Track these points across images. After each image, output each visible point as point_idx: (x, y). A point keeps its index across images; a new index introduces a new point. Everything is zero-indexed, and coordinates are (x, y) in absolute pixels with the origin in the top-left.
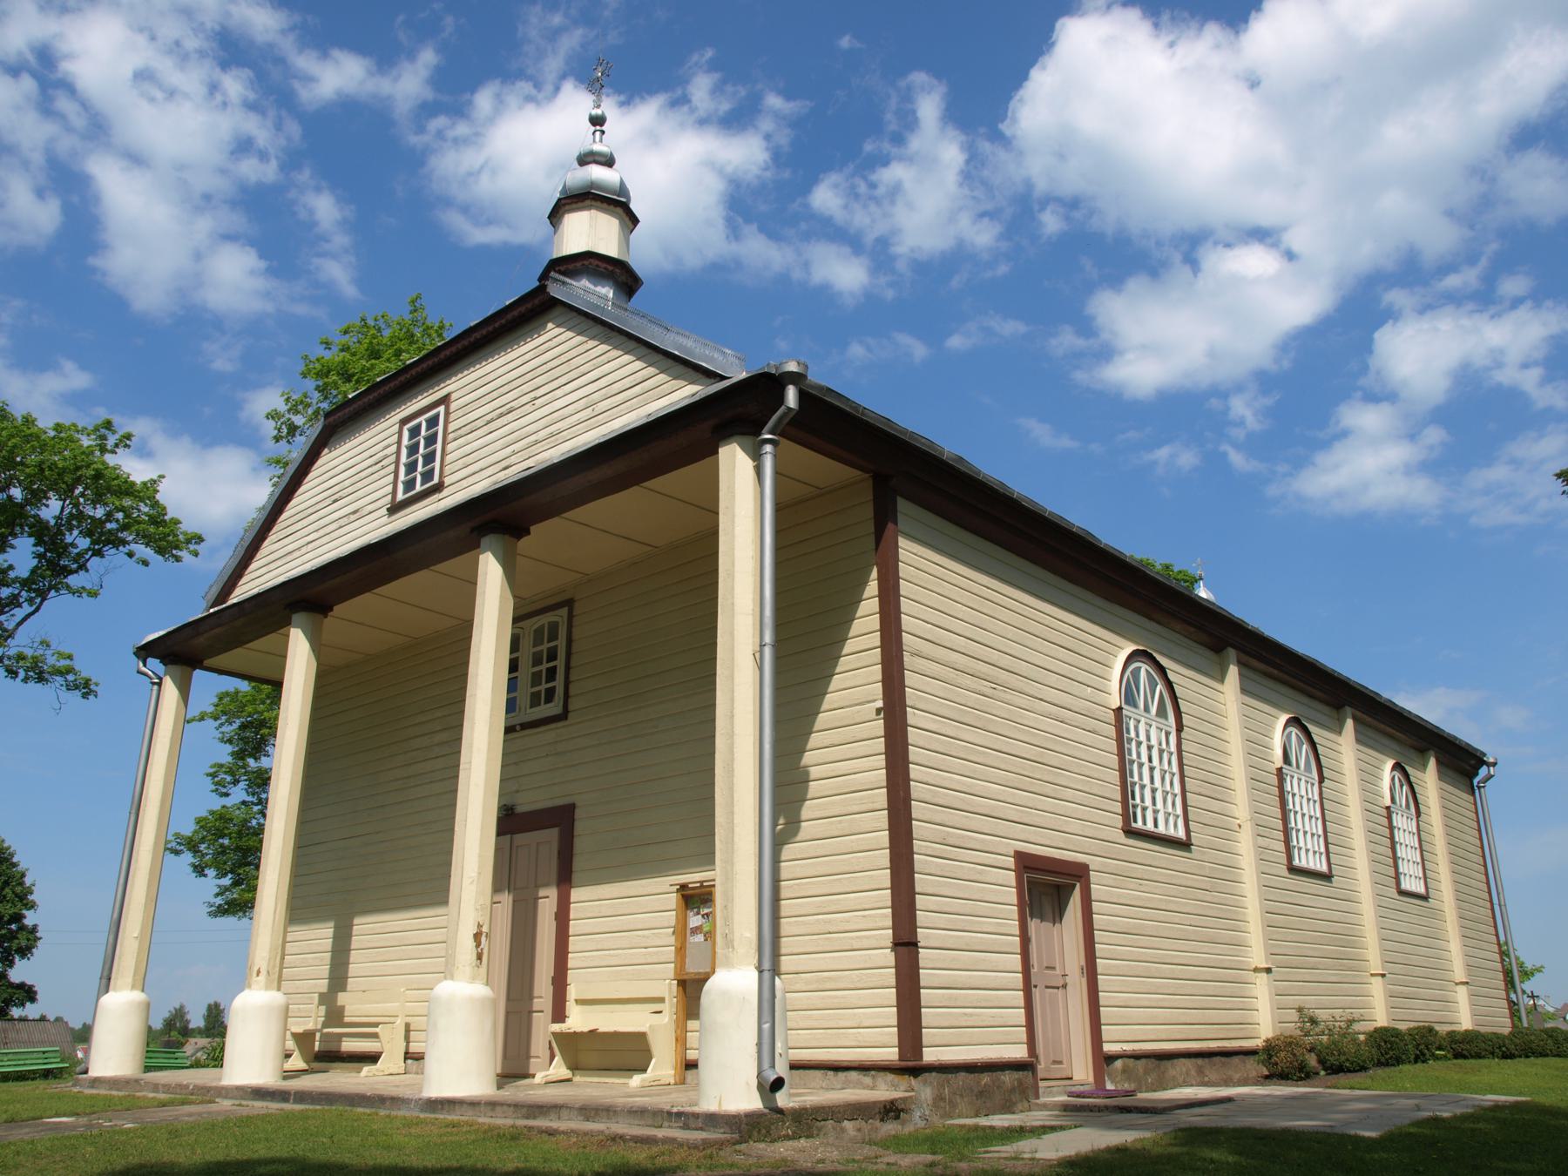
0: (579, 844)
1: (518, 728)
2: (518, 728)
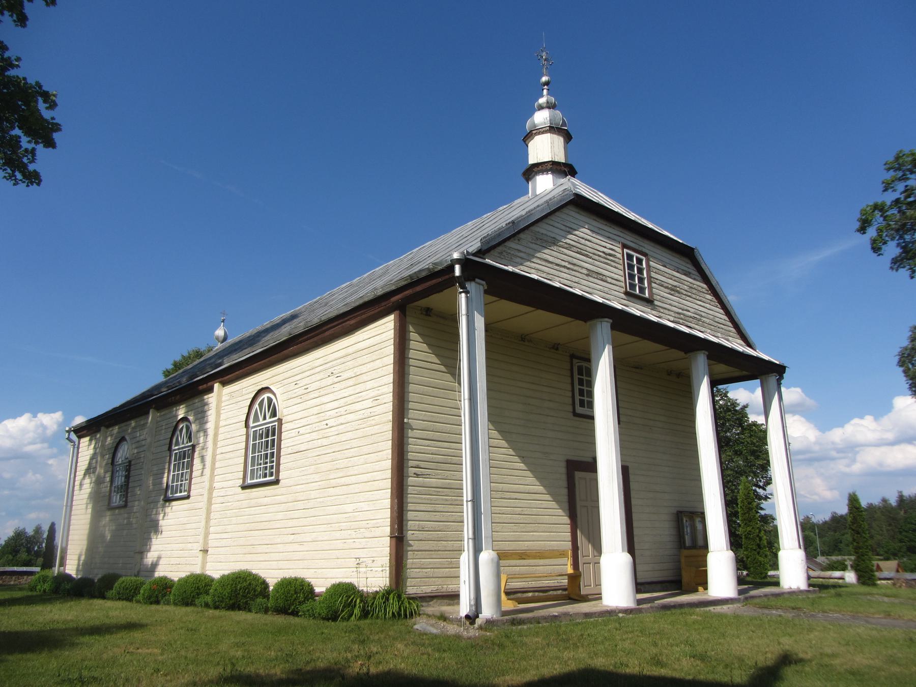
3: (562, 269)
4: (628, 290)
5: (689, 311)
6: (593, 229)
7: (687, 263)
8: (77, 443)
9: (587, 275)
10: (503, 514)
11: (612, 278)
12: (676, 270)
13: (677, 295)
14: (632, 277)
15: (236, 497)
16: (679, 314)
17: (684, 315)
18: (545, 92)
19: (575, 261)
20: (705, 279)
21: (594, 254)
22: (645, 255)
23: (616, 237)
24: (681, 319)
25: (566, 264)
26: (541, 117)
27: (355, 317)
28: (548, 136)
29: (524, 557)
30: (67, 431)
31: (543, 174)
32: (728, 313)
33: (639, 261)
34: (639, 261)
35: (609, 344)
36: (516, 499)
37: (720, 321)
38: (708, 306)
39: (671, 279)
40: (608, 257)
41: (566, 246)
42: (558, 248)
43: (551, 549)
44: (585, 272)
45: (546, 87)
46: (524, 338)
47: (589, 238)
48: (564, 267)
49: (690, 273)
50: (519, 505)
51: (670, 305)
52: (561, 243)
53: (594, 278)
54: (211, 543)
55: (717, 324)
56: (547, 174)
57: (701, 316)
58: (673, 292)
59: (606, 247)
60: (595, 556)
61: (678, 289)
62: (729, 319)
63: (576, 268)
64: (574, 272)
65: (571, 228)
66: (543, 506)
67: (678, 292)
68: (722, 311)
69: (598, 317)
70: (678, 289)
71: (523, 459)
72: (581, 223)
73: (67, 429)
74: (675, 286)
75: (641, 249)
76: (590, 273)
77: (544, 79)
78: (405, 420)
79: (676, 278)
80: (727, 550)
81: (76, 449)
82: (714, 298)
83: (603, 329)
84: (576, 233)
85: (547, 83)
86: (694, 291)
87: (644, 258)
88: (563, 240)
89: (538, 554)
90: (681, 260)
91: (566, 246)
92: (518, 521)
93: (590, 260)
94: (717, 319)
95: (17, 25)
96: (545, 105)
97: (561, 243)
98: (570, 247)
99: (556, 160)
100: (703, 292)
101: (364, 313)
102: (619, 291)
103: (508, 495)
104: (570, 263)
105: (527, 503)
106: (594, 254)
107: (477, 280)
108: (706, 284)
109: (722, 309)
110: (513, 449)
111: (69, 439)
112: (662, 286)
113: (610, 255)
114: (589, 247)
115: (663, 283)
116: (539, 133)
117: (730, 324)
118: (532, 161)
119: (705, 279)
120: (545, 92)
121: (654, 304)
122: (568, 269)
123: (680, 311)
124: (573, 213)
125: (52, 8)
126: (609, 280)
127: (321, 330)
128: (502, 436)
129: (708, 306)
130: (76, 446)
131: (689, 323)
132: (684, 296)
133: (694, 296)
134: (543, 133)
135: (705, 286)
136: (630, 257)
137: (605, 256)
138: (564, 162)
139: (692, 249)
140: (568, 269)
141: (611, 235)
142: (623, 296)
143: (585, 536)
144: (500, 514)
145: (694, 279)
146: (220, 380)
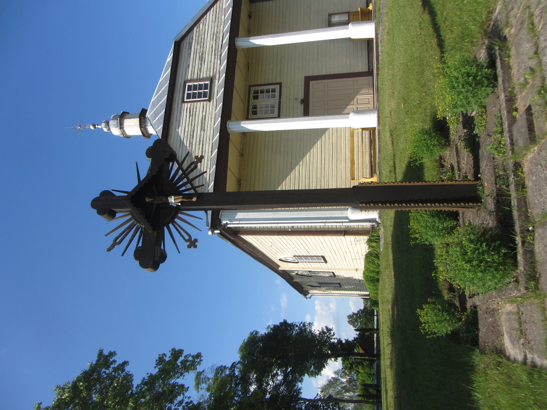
0: (315, 74)
1: (280, 100)
2: (280, 100)
3: (204, 150)
4: (207, 99)
5: (212, 45)
6: (177, 126)
7: (184, 45)
8: (312, 294)
9: (204, 131)
10: (332, 169)
11: (203, 111)
12: (189, 55)
13: (204, 56)
14: (200, 95)
15: (331, 263)
16: (215, 54)
17: (215, 50)
18: (99, 127)
19: (198, 140)
20: (191, 30)
21: (192, 125)
22: (185, 83)
23: (179, 108)
24: (218, 53)
25: (201, 146)
26: (116, 131)
27: (242, 245)
28: (125, 129)
29: (353, 162)
30: (307, 299)
31: (148, 130)
32: (209, 10)
33: (189, 89)
34: (190, 88)
35: (240, 124)
36: (325, 160)
37: (215, 12)
38: (207, 27)
39: (196, 60)
40: (191, 114)
41: (191, 147)
42: (193, 152)
43: (350, 136)
44: (202, 132)
45: (96, 126)
46: (242, 155)
47: (183, 128)
48: (202, 148)
49: (189, 43)
50: (328, 158)
51: (211, 62)
52: (190, 150)
53: (205, 126)
54: (353, 267)
55: (217, 20)
56: (147, 128)
57: (214, 34)
58: (203, 59)
59: (186, 116)
60: (354, 104)
61: (200, 55)
62: (212, 8)
63: (202, 139)
64: (204, 141)
65: (180, 142)
66: (328, 141)
67: (202, 54)
68: (208, 14)
69: (227, 131)
70: (200, 55)
71: (304, 155)
72: (176, 134)
73: (305, 299)
74: (199, 57)
75: (182, 87)
76: (203, 129)
77: (92, 128)
78: (290, 230)
79: (195, 56)
80: (348, 28)
81: (314, 294)
82: (201, 21)
83: (233, 127)
84: (182, 138)
85: (94, 126)
86: (200, 40)
87: (187, 84)
88: (188, 148)
89: (352, 152)
90: (183, 50)
91: (191, 147)
92: (336, 160)
93: (195, 127)
94: (214, 19)
95: (128, 364)
96: (108, 128)
97: (190, 150)
98: (191, 144)
99: (139, 124)
100: (199, 31)
101: (241, 244)
102: (210, 106)
103: (323, 165)
104: (199, 144)
105: (327, 153)
106: (192, 125)
107: (220, 218)
108: (194, 28)
109: (207, 13)
110: (300, 162)
111: (310, 298)
112: (201, 69)
113: (190, 112)
114: (188, 129)
115: (199, 68)
116: (125, 133)
117: (215, 6)
118: (141, 134)
119: (191, 30)
120: (99, 127)
121: (213, 76)
122: (203, 145)
123: (213, 53)
124: (172, 140)
125: (117, 352)
126: (204, 114)
127: (249, 252)
128: (294, 169)
129: (207, 27)
130: (313, 294)
131: (220, 44)
132: (204, 49)
133: (203, 40)
134: (124, 131)
135: (195, 29)
136: (189, 96)
137: (191, 116)
138: (138, 119)
139: (175, 42)
140: (203, 145)
141: (179, 113)
142: (211, 102)
143: (343, 111)
144: (332, 171)
145: (192, 39)
146: (277, 269)
